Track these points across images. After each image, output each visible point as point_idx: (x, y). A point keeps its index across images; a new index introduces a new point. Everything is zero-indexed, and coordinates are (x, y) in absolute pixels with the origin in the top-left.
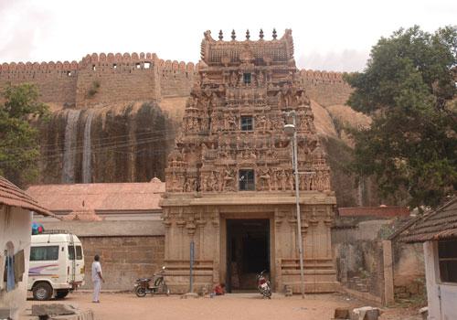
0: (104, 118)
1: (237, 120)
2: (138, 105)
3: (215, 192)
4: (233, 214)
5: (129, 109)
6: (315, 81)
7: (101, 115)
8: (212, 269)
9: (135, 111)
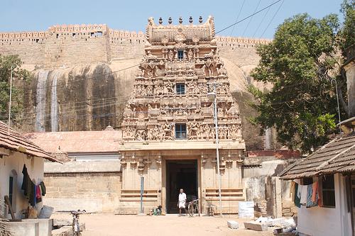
0: (67, 77)
1: (173, 87)
2: (93, 68)
3: (158, 140)
4: (171, 157)
5: (86, 70)
6: (232, 46)
7: (64, 76)
8: (156, 196)
9: (90, 72)
